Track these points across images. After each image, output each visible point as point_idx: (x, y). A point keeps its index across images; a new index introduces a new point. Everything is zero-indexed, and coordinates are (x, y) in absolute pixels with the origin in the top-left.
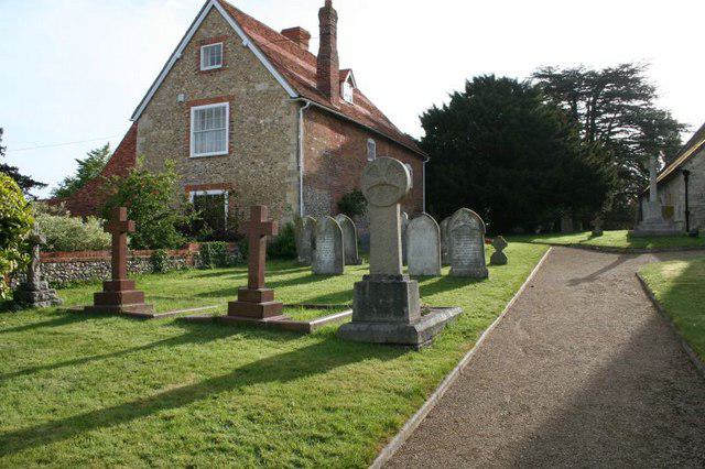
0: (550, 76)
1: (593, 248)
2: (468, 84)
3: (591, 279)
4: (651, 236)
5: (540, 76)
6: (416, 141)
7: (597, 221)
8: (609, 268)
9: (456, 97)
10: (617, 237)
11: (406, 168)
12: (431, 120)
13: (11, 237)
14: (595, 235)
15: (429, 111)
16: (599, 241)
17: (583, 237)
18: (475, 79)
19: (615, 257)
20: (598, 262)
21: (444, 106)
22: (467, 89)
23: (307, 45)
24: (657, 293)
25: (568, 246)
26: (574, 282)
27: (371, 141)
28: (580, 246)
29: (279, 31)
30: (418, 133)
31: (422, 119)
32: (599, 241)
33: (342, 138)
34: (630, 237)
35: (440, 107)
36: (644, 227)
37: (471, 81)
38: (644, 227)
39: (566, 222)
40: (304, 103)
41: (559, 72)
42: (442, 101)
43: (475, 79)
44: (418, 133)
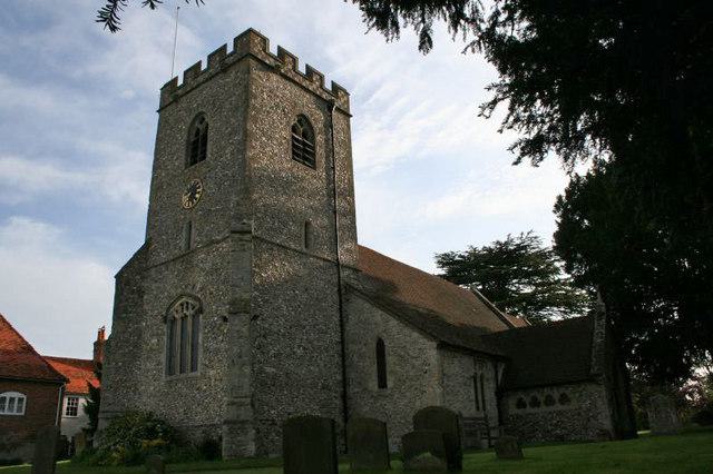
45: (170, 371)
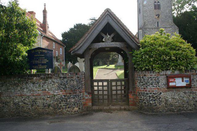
0: (95, 20)
1: (107, 69)
2: (75, 26)
3: (107, 74)
4: (119, 66)
5: (92, 20)
6: (60, 40)
7: (108, 63)
8: (112, 72)
9: (71, 29)
10: (112, 66)
11: (61, 49)
12: (65, 35)
13: (27, 83)
14: (108, 66)
15: (64, 33)
16: (108, 67)
17: (105, 66)
18: (77, 24)
19: (112, 70)
20: (108, 71)
21: (68, 31)
22: (74, 27)
23: (35, 16)
24: (118, 75)
25: (102, 68)
26: (104, 75)
27: (54, 43)
28: (105, 68)
29: (58, 29)
30: (60, 38)
31: (62, 35)
32: (108, 67)
33: (48, 43)
34: (115, 66)
35: (67, 32)
36: (118, 64)
37: (75, 25)
38: (118, 64)
39: (101, 63)
40: (42, 35)
41: (97, 19)
42: (67, 30)
43: (77, 24)
44: (60, 38)
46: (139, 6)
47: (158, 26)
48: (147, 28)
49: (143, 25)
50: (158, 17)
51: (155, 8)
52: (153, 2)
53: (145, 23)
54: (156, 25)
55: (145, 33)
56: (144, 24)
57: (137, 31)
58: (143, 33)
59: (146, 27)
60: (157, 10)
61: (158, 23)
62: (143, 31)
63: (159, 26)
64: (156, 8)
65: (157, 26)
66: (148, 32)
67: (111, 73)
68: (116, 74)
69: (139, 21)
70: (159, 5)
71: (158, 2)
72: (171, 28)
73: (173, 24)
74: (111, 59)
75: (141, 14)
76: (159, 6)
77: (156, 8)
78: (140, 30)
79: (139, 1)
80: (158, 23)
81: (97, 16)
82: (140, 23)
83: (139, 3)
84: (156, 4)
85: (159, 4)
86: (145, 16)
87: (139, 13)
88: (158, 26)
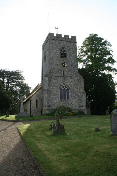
1: (6, 120)
3: (4, 130)
8: (11, 125)
10: (12, 117)
16: (8, 118)
19: (11, 123)
20: (6, 125)
24: (22, 133)
34: (16, 117)
36: (20, 114)
38: (20, 114)
45: (61, 98)
46: (44, 53)
47: (64, 75)
48: (53, 76)
49: (48, 72)
50: (64, 65)
51: (61, 57)
52: (60, 50)
53: (51, 71)
54: (62, 74)
55: (50, 81)
56: (50, 72)
57: (39, 81)
58: (48, 81)
59: (52, 74)
60: (63, 58)
61: (64, 71)
62: (49, 78)
63: (65, 75)
64: (63, 56)
65: (63, 75)
66: (54, 80)
67: (9, 128)
68: (18, 130)
69: (44, 69)
70: (65, 53)
71: (64, 51)
72: (76, 78)
73: (78, 74)
74: (11, 109)
75: (47, 61)
76: (65, 55)
77: (63, 56)
78: (46, 77)
79: (44, 49)
80: (64, 71)
81: (28, 85)
82: (44, 72)
83: (44, 51)
84: (62, 52)
85: (65, 52)
86: (51, 64)
87: (44, 61)
88: (64, 75)
